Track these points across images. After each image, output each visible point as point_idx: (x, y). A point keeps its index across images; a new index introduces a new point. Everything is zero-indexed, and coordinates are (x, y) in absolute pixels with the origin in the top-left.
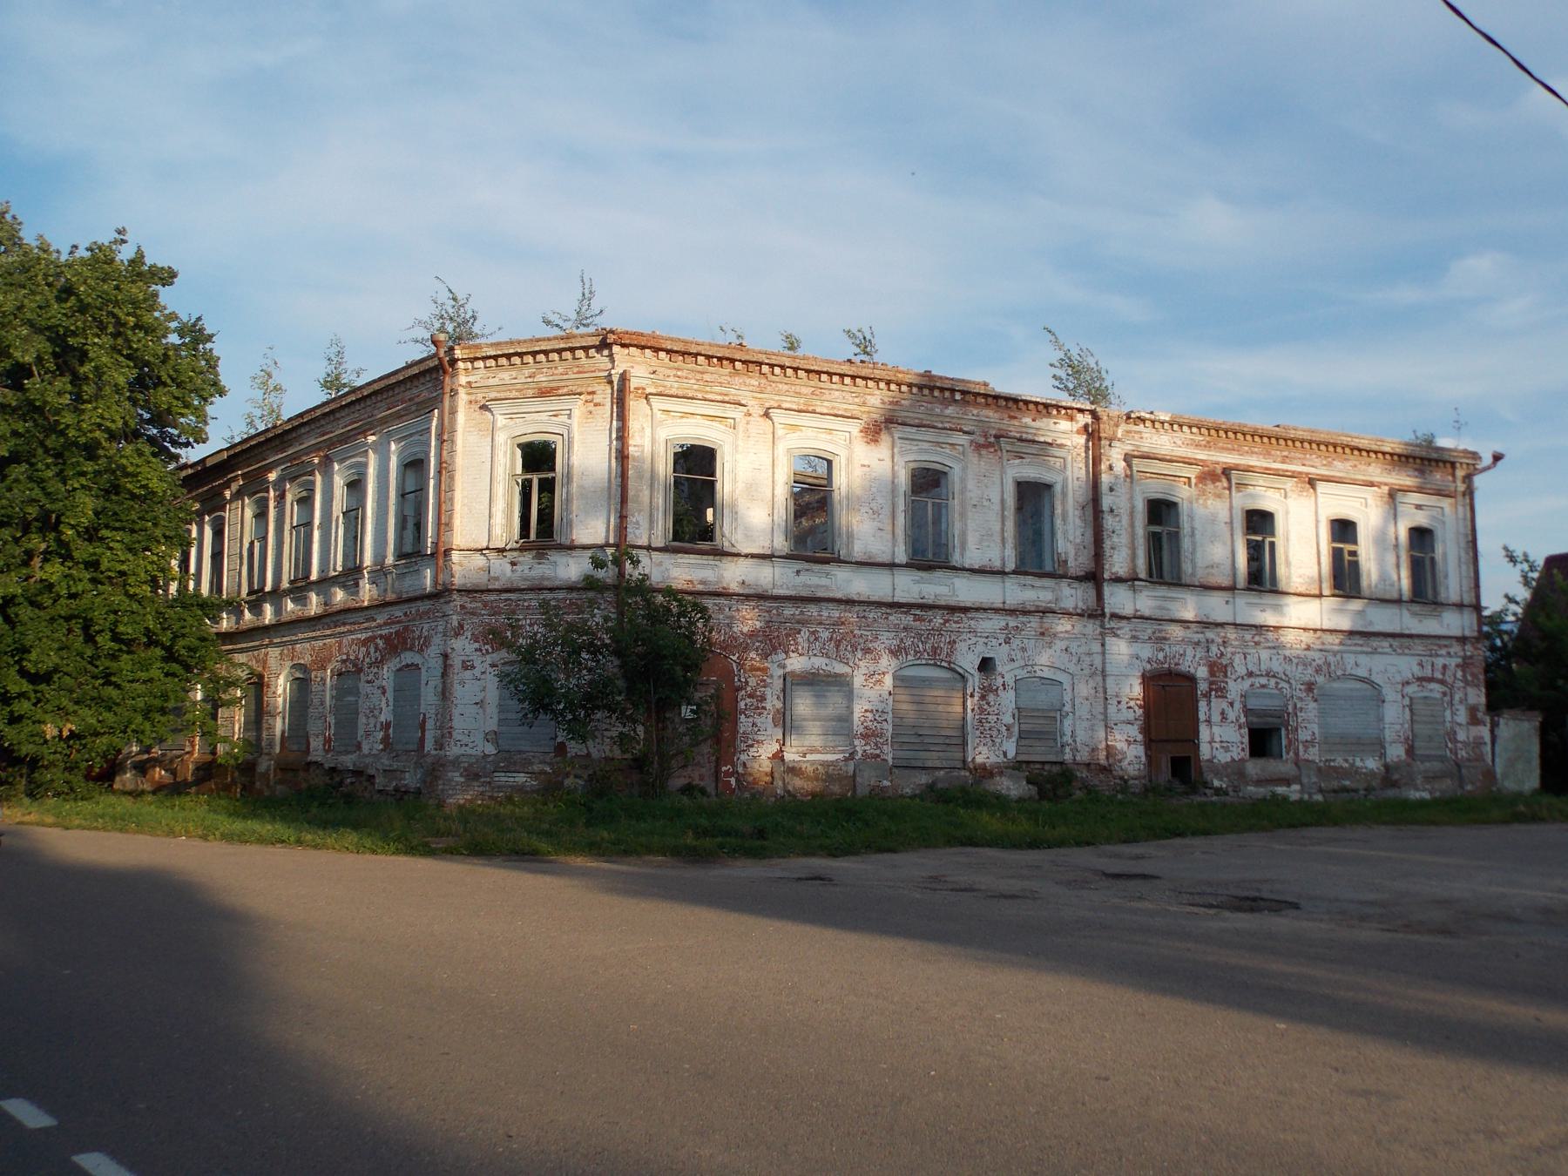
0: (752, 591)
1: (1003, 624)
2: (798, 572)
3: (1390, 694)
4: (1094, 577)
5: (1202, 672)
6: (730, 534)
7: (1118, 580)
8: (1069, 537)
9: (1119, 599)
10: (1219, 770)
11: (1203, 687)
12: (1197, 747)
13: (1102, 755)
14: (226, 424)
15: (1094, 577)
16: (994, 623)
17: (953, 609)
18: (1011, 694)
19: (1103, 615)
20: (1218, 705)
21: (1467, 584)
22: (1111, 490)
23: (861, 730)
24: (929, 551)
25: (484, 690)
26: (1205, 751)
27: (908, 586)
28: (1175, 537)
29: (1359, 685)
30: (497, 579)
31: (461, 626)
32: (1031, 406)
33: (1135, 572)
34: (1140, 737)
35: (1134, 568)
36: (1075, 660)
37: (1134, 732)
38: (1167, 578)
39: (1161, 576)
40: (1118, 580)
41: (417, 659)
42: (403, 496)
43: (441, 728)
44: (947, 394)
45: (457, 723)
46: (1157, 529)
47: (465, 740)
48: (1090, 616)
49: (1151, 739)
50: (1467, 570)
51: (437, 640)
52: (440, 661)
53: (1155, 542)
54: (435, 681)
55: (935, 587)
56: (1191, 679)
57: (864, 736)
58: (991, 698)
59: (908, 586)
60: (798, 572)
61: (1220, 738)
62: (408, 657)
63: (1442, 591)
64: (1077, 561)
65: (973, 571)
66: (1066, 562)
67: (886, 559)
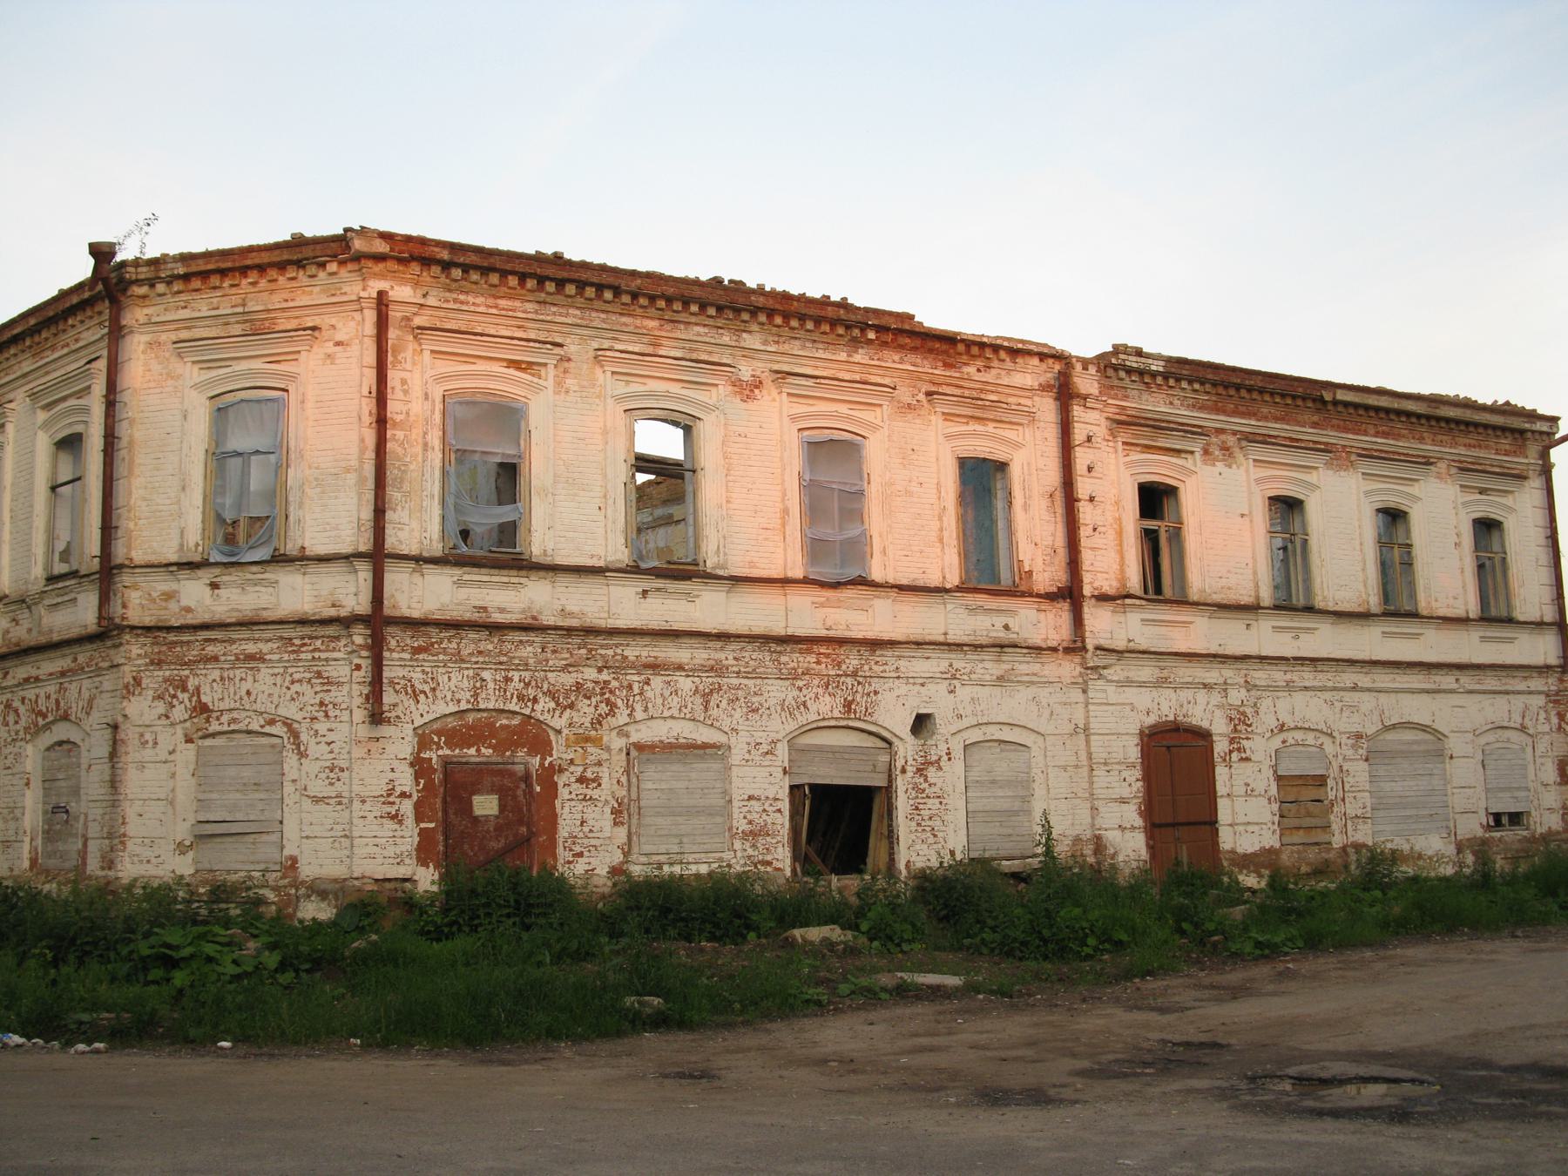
0: (574, 623)
1: (944, 665)
2: (645, 592)
3: (1455, 744)
4: (1070, 594)
5: (1219, 727)
6: (545, 535)
7: (1103, 598)
8: (1033, 537)
9: (1102, 624)
10: (1248, 861)
11: (1220, 746)
12: (1215, 832)
13: (1088, 851)
14: (1129, 846)
15: (1070, 594)
16: (936, 664)
17: (875, 645)
18: (958, 766)
19: (1084, 649)
20: (1243, 772)
21: (1547, 594)
22: (1090, 469)
23: (743, 826)
24: (838, 566)
25: (173, 775)
26: (1227, 840)
27: (805, 614)
28: (1177, 535)
29: (1421, 736)
30: (188, 610)
31: (138, 682)
32: (961, 347)
33: (1258, 598)
34: (1139, 822)
35: (1123, 580)
36: (1046, 713)
37: (1132, 815)
38: (1168, 591)
39: (1158, 589)
40: (1103, 598)
41: (72, 734)
42: (53, 489)
43: (110, 836)
44: (856, 332)
45: (133, 828)
46: (1152, 524)
47: (148, 853)
48: (1067, 650)
49: (1157, 823)
50: (1545, 575)
51: (103, 702)
52: (108, 733)
53: (1150, 539)
54: (101, 771)
55: (509, 597)
56: (1204, 736)
57: (745, 835)
58: (931, 772)
59: (624, 604)
60: (645, 592)
61: (1246, 821)
62: (61, 731)
63: (1517, 602)
64: (1048, 575)
65: (901, 588)
66: (1030, 573)
67: (1246, 599)
